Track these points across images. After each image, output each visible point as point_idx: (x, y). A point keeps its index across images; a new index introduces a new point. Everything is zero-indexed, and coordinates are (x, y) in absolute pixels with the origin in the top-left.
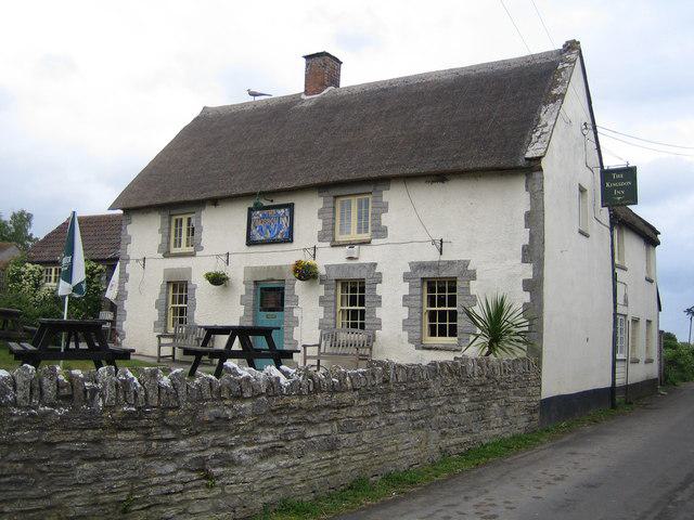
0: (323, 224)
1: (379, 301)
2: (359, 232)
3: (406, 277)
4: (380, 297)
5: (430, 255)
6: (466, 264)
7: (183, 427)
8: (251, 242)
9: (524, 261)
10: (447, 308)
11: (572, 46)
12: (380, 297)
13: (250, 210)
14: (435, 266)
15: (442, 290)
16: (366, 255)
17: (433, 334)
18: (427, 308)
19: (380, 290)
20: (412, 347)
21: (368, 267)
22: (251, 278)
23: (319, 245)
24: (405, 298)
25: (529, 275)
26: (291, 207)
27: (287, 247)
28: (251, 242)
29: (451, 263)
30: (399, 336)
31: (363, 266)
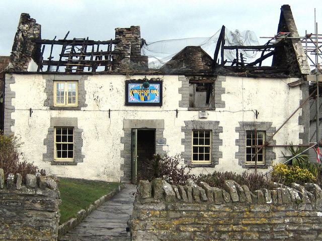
0: (182, 97)
1: (220, 142)
2: (70, 102)
3: (237, 130)
4: (222, 140)
5: (250, 118)
6: (270, 124)
7: (151, 217)
8: (127, 104)
9: (300, 124)
10: (62, 143)
11: (26, 19)
12: (222, 140)
13: (127, 83)
14: (253, 124)
15: (202, 135)
16: (211, 116)
17: (59, 156)
18: (193, 145)
19: (221, 136)
20: (241, 167)
21: (213, 123)
22: (128, 126)
23: (179, 109)
24: (237, 141)
25: (302, 131)
26: (160, 83)
27: (157, 108)
28: (127, 104)
29: (263, 123)
30: (233, 161)
31: (210, 123)
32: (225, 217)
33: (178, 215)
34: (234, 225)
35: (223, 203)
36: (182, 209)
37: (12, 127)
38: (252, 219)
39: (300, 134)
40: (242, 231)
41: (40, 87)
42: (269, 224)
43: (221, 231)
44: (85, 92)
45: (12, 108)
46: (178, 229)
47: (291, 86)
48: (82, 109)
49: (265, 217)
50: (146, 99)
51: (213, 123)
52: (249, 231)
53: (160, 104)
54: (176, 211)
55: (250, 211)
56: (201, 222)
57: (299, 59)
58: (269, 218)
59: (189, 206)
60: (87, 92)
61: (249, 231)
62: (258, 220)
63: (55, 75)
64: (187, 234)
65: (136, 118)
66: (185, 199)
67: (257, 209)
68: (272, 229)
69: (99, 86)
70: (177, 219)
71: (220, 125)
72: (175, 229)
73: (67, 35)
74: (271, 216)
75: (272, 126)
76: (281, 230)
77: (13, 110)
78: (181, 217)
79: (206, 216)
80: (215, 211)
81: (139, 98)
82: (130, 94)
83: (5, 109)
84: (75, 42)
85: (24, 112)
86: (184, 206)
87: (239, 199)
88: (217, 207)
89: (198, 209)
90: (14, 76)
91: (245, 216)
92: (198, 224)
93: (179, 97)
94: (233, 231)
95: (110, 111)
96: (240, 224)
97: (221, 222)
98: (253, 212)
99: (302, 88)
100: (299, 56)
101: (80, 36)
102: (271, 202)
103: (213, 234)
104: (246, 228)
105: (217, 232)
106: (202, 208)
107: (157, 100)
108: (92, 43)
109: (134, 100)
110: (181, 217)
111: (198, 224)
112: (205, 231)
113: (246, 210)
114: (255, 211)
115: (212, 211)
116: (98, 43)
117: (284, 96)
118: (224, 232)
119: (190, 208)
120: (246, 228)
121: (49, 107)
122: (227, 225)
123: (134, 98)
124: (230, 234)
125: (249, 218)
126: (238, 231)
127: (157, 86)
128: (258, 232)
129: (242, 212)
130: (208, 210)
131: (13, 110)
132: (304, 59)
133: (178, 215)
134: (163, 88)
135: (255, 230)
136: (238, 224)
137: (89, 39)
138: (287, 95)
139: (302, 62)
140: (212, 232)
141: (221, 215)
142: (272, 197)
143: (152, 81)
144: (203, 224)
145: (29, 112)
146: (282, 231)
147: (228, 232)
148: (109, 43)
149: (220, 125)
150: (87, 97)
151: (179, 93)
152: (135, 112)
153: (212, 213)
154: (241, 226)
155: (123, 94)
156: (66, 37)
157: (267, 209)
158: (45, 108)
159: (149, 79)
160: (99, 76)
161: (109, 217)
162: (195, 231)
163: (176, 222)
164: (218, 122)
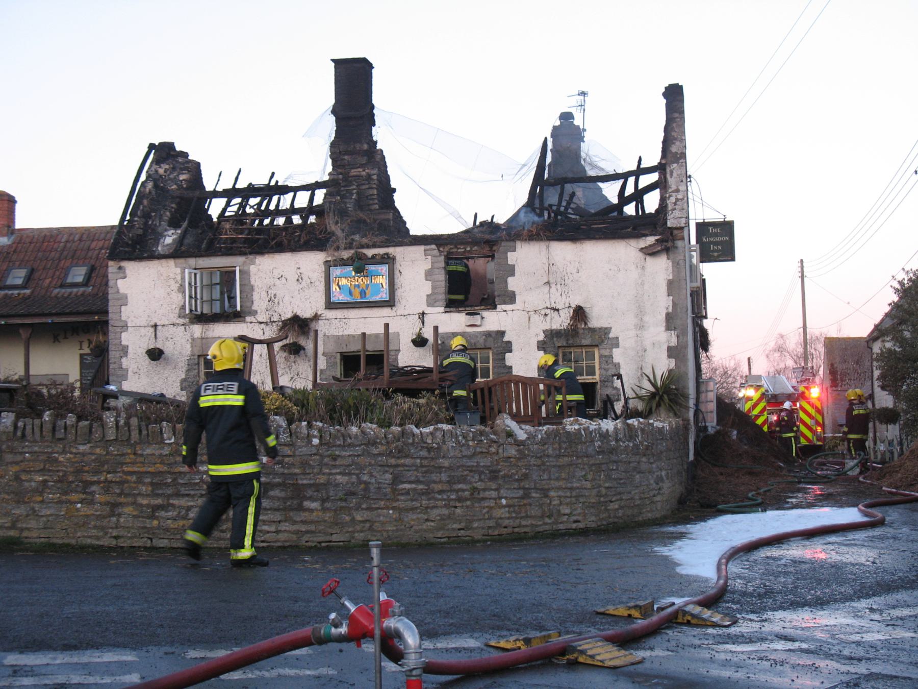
9: (668, 328)
16: (492, 320)
21: (493, 335)
23: (428, 310)
25: (674, 342)
26: (388, 260)
32: (94, 461)
33: (19, 458)
34: (109, 473)
35: (88, 443)
36: (24, 450)
37: (124, 360)
38: (138, 465)
39: (670, 349)
40: (121, 483)
41: (172, 282)
42: (169, 473)
43: (86, 481)
44: (252, 288)
45: (122, 324)
46: (17, 478)
47: (650, 252)
48: (248, 319)
49: (162, 463)
50: (363, 293)
51: (493, 335)
52: (135, 483)
53: (390, 303)
54: (15, 453)
55: (135, 454)
56: (54, 468)
57: (670, 196)
58: (169, 464)
59: (36, 446)
60: (256, 288)
61: (135, 483)
62: (149, 467)
63: (197, 259)
64: (33, 484)
65: (346, 333)
66: (29, 437)
67: (148, 451)
68: (174, 480)
69: (277, 273)
70: (17, 463)
71: (505, 339)
72: (13, 477)
73: (237, 179)
74: (173, 461)
75: (611, 335)
76: (193, 481)
77: (125, 327)
78: (22, 461)
79: (62, 459)
80: (76, 454)
81: (351, 293)
82: (334, 287)
83: (110, 328)
84: (252, 191)
85: (143, 331)
86: (27, 446)
87: (117, 436)
88: (82, 448)
89: (50, 450)
90: (124, 264)
91: (128, 460)
92: (50, 471)
93: (427, 288)
94: (106, 481)
95: (155, 326)
96: (119, 472)
97: (86, 468)
98: (142, 455)
99: (671, 256)
100: (673, 192)
101: (261, 180)
102: (173, 441)
103: (73, 485)
104: (129, 478)
105: (80, 482)
106: (56, 449)
107: (384, 295)
108: (283, 190)
109: (341, 298)
110: (22, 461)
111: (50, 471)
112: (60, 481)
113: (129, 451)
114: (145, 453)
115: (71, 453)
116: (295, 190)
117: (634, 274)
118: (93, 483)
119: (36, 449)
120: (129, 478)
121: (187, 320)
122: (97, 472)
123: (340, 294)
124: (102, 485)
125: (133, 463)
126: (115, 482)
127: (384, 269)
128: (152, 484)
129: (123, 455)
130: (64, 452)
131: (125, 327)
132: (680, 197)
133: (19, 458)
134: (397, 272)
135: (148, 480)
136: (115, 472)
137: (279, 184)
138: (640, 270)
139: (675, 204)
140: (72, 482)
141: (86, 459)
142: (174, 434)
143: (375, 260)
144: (58, 471)
145: (152, 330)
146: (197, 484)
147: (98, 482)
148: (312, 188)
149: (505, 339)
150: (256, 296)
151: (427, 280)
152: (344, 320)
153: (72, 456)
154: (121, 475)
155: (322, 287)
156: (235, 183)
157: (166, 451)
158: (181, 321)
159: (370, 256)
160: (164, 261)
161: (914, 618)
162: (45, 481)
163: (13, 469)
164: (503, 333)
